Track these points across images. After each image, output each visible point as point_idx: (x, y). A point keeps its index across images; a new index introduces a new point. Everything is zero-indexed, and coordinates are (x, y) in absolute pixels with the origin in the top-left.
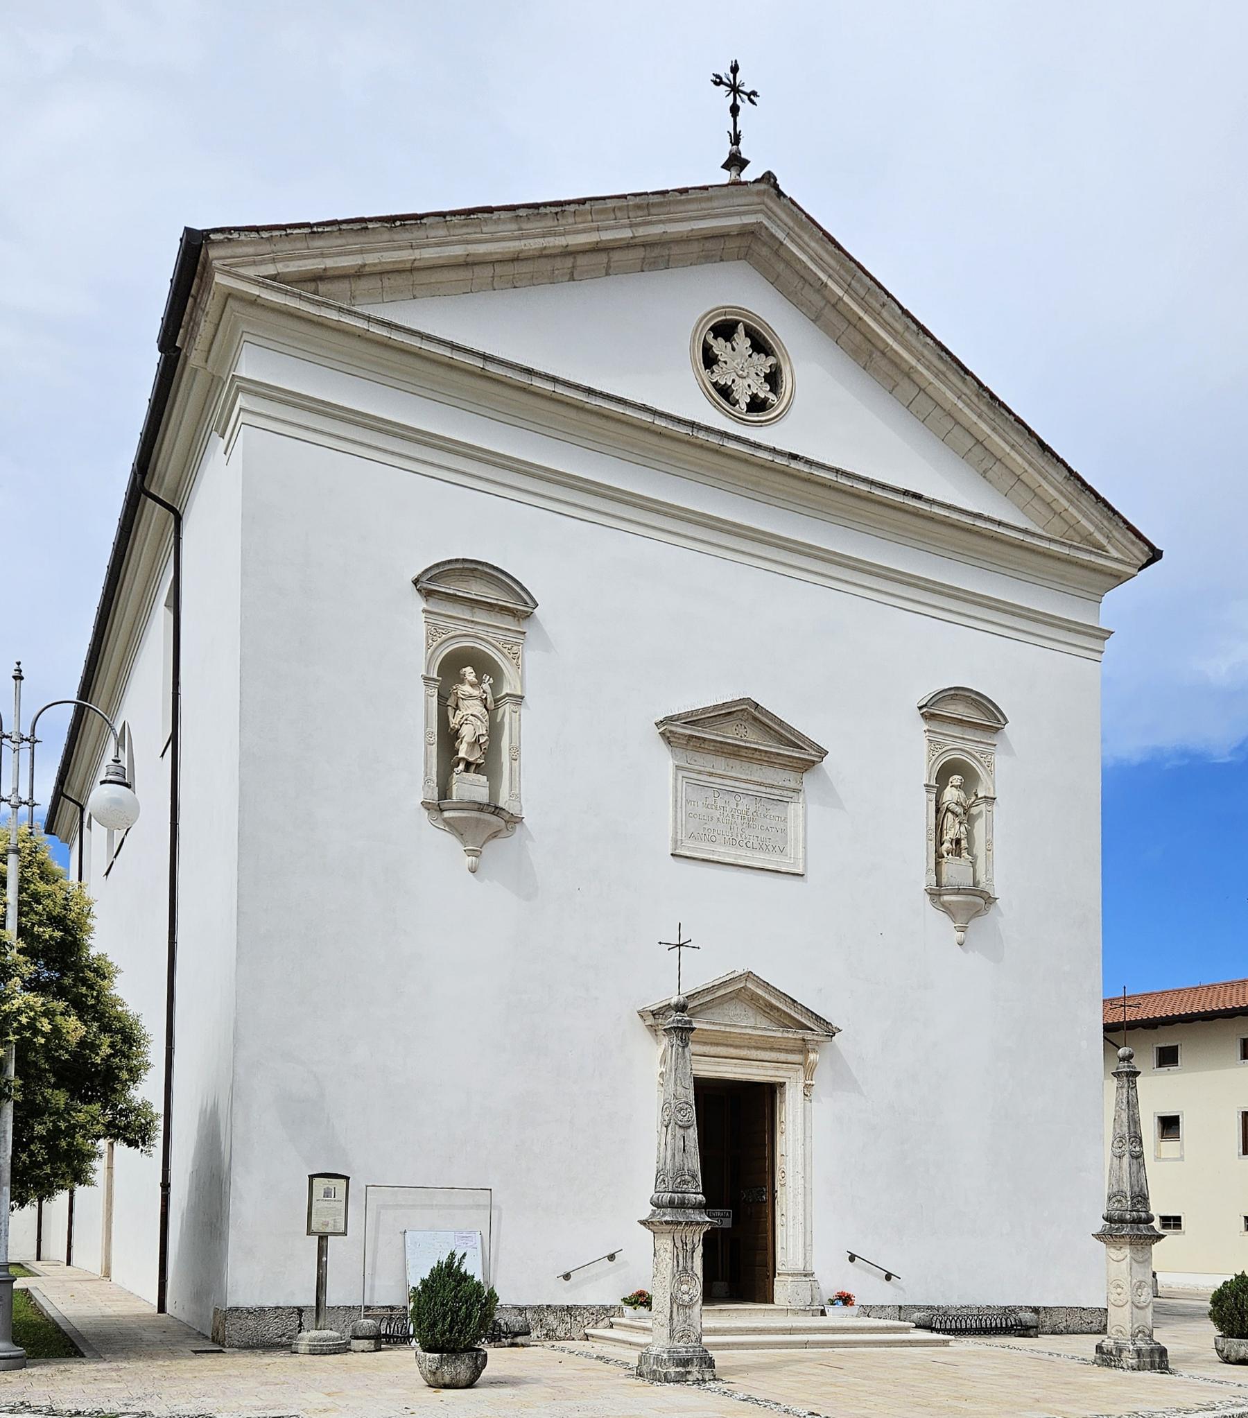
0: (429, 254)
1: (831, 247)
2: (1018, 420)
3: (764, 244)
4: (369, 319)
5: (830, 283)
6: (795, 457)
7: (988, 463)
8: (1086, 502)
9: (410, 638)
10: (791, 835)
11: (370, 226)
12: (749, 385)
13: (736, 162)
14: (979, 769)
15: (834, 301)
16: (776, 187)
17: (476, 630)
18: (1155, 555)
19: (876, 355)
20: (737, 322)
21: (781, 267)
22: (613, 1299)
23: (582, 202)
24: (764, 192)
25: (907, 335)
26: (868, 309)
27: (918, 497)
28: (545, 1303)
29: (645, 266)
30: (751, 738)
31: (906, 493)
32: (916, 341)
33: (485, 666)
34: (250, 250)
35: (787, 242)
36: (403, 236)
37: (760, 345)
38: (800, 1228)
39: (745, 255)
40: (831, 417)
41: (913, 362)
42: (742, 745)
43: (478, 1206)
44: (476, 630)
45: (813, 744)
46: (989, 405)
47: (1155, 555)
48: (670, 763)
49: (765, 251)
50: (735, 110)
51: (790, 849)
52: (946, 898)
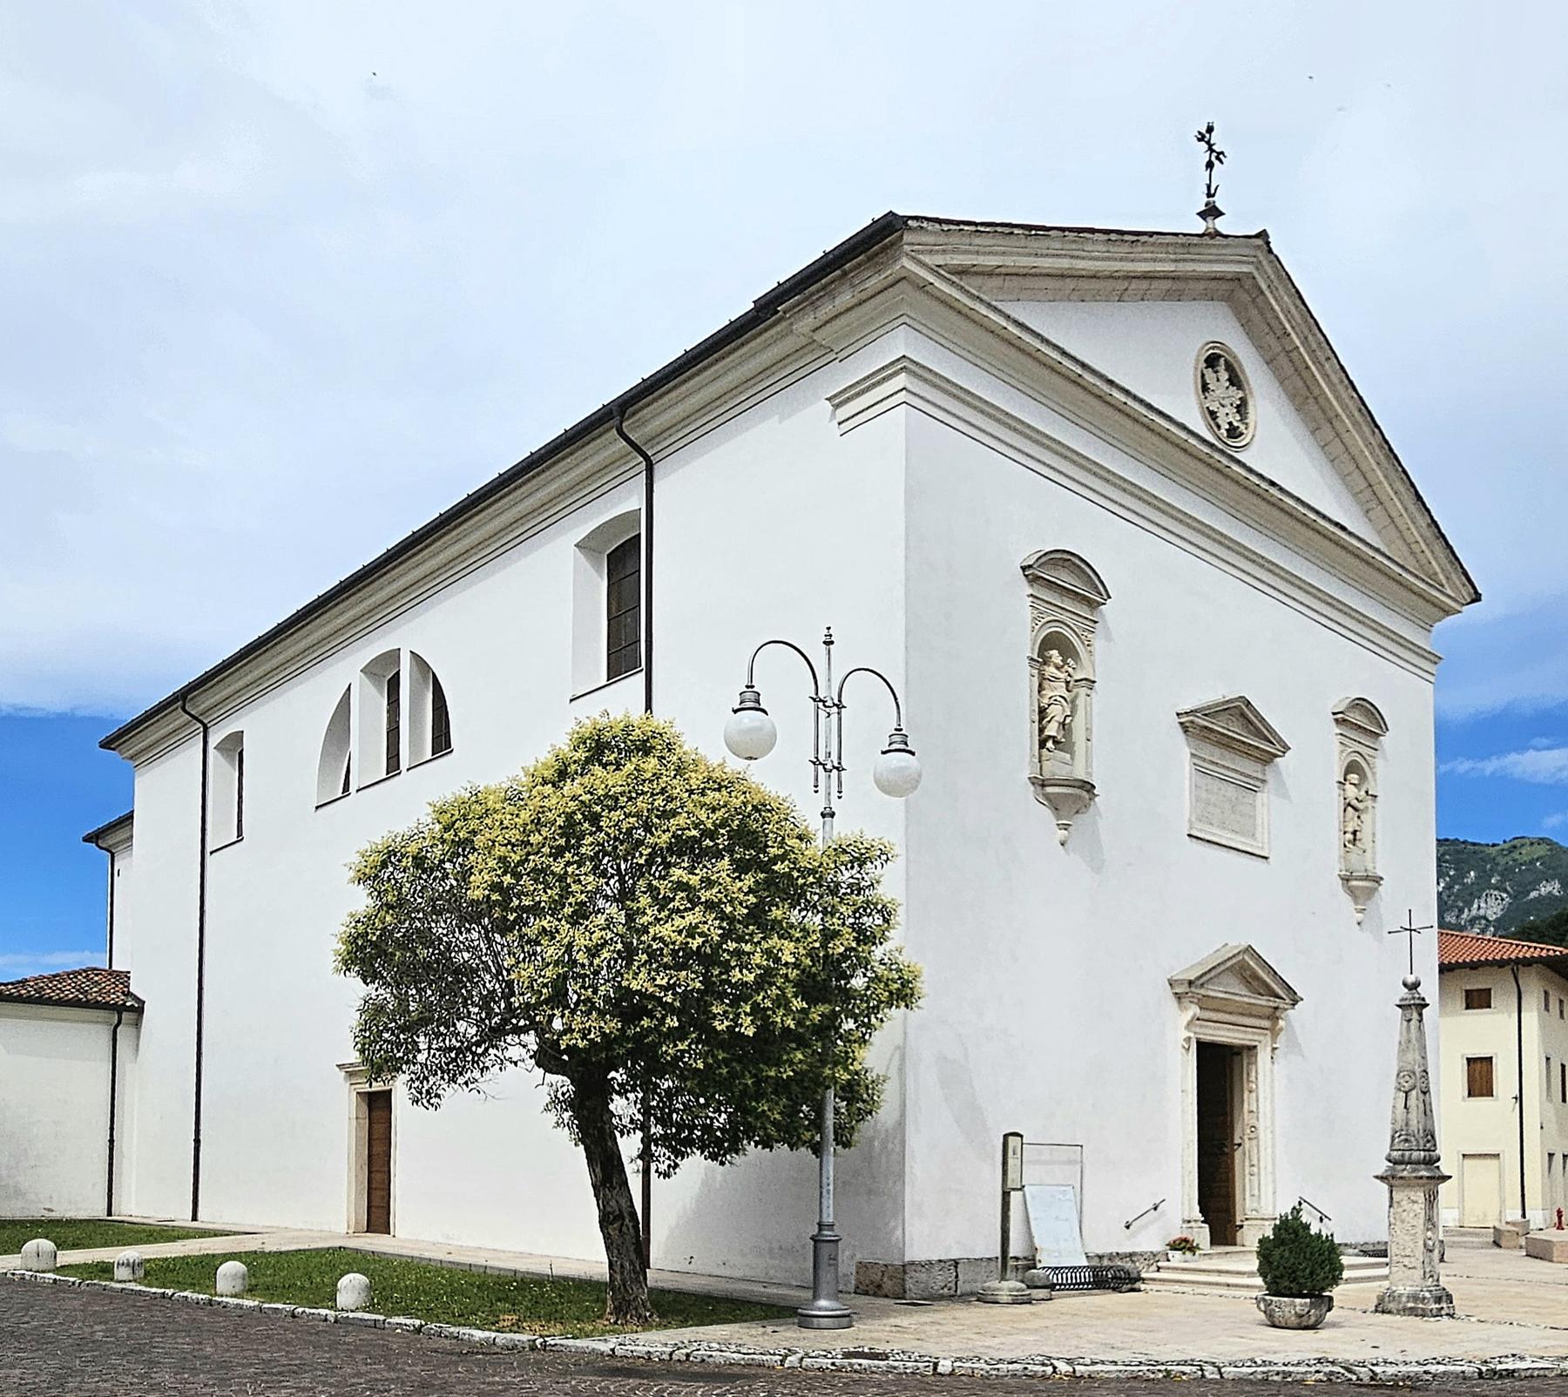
0: (1046, 263)
1: (1299, 302)
2: (1404, 472)
3: (1247, 292)
4: (1008, 317)
5: (1293, 335)
6: (1273, 484)
7: (1373, 504)
8: (1438, 547)
9: (1018, 618)
10: (1259, 821)
11: (1016, 231)
12: (1227, 416)
13: (1211, 212)
14: (1369, 774)
15: (1289, 348)
16: (1268, 243)
17: (1064, 617)
18: (1477, 597)
19: (1311, 400)
20: (1220, 356)
21: (1254, 312)
22: (1158, 1246)
23: (1151, 234)
24: (1259, 247)
25: (1339, 387)
26: (1316, 362)
27: (1343, 528)
28: (1114, 1251)
29: (1167, 296)
30: (1235, 730)
31: (1337, 524)
32: (1345, 394)
33: (1068, 651)
34: (931, 239)
35: (1267, 293)
36: (1034, 244)
37: (1235, 381)
38: (1270, 1177)
39: (1228, 298)
40: (1278, 447)
41: (1340, 411)
42: (1234, 736)
43: (1070, 1162)
44: (1064, 617)
45: (1280, 741)
46: (1387, 457)
47: (1477, 597)
48: (1187, 751)
49: (1245, 297)
50: (1210, 165)
51: (1258, 835)
52: (1354, 883)
